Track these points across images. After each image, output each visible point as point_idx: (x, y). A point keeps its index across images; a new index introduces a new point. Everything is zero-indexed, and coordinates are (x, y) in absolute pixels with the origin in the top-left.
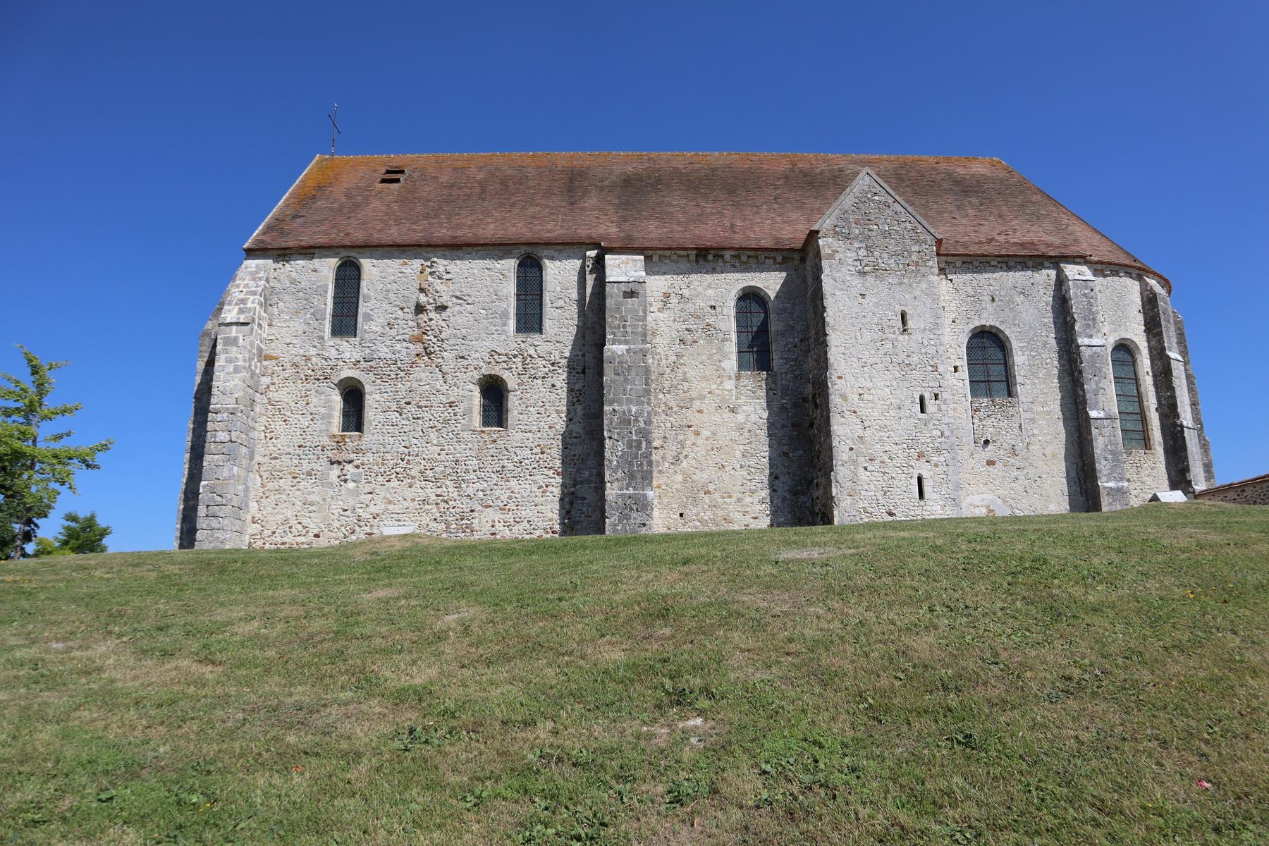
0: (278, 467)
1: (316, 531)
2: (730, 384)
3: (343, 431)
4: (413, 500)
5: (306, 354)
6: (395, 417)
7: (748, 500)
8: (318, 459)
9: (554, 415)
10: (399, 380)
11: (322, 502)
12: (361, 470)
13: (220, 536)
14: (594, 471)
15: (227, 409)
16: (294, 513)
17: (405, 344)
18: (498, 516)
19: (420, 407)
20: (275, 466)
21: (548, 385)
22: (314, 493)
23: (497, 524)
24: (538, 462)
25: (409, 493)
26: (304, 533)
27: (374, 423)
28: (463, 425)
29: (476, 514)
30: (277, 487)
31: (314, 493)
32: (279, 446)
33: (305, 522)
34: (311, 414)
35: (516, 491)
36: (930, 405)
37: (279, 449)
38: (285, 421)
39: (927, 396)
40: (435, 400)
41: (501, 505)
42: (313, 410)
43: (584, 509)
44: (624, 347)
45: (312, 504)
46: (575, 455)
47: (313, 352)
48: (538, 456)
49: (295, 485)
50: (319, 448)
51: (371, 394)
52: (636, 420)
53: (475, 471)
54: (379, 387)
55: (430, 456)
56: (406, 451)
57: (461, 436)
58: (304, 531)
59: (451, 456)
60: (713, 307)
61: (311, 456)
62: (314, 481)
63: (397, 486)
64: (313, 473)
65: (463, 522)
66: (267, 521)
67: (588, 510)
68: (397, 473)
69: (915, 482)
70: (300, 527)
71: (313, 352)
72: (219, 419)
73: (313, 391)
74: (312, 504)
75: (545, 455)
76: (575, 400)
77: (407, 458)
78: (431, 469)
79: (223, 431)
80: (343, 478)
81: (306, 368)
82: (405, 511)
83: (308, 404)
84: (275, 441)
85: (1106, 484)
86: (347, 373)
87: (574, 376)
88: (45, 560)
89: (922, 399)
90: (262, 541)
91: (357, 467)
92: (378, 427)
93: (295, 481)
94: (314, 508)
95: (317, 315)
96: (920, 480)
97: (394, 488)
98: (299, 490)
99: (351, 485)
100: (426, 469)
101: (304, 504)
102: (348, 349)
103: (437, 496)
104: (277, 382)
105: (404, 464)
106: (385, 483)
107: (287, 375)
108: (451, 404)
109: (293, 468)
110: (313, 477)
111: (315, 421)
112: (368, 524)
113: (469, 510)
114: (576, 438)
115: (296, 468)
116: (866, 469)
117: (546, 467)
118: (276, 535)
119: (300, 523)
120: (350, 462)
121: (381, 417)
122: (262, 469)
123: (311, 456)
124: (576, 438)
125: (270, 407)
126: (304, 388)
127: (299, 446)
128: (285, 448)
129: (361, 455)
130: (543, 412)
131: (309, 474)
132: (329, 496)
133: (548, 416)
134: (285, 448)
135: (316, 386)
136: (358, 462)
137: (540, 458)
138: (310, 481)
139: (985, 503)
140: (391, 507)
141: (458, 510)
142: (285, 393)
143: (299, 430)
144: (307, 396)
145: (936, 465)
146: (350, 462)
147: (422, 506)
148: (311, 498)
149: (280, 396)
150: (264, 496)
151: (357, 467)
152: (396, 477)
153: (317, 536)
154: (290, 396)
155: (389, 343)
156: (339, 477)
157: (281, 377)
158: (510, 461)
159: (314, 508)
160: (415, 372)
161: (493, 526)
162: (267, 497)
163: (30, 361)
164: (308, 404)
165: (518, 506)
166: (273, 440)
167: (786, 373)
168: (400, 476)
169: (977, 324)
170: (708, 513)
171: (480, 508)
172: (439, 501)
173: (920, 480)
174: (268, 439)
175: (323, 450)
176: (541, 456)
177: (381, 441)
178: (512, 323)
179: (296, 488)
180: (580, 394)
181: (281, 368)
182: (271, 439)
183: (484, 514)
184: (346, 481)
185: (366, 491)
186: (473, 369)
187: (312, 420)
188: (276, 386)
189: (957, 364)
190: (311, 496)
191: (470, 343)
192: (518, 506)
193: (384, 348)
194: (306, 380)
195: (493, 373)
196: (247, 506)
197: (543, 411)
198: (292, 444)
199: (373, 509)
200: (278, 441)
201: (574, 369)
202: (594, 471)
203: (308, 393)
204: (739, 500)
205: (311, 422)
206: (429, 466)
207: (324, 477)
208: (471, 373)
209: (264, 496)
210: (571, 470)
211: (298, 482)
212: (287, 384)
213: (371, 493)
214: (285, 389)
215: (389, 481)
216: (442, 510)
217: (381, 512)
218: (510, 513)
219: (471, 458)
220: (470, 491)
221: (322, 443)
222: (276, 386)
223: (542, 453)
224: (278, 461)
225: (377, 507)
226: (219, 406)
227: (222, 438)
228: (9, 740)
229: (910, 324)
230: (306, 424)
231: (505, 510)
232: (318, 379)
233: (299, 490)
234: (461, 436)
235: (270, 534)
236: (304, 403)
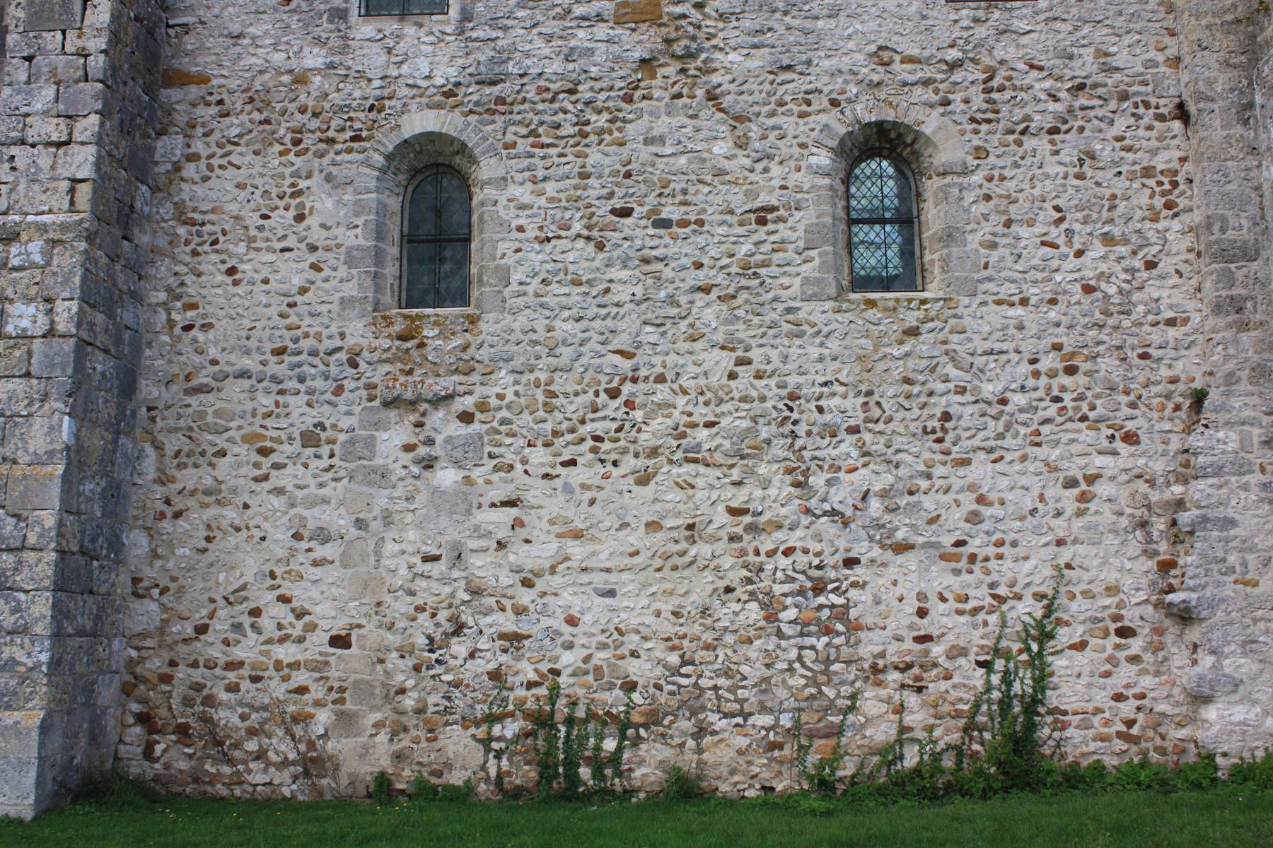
0: (210, 419)
1: (339, 627)
4: (653, 526)
5: (293, 64)
6: (578, 255)
8: (339, 390)
9: (1098, 250)
10: (593, 138)
11: (354, 532)
12: (476, 427)
13: (21, 656)
14: (1256, 431)
15: (43, 228)
16: (267, 568)
17: (602, 31)
18: (941, 578)
19: (664, 224)
20: (202, 415)
21: (1069, 153)
22: (325, 501)
23: (936, 608)
24: (1057, 399)
25: (640, 504)
26: (297, 632)
27: (516, 276)
28: (806, 281)
29: (859, 573)
30: (208, 482)
31: (325, 501)
32: (213, 352)
33: (299, 592)
34: (313, 249)
35: (993, 496)
37: (214, 362)
38: (232, 271)
40: (709, 200)
41: (947, 540)
42: (317, 236)
43: (1233, 559)
45: (323, 536)
46: (1174, 380)
47: (314, 58)
48: (1055, 383)
49: (266, 478)
50: (342, 356)
53: (854, 430)
54: (526, 162)
55: (702, 381)
56: (625, 365)
57: (802, 315)
58: (300, 624)
59: (772, 382)
61: (319, 384)
62: (325, 462)
63: (597, 481)
64: (323, 436)
65: (821, 600)
66: (181, 590)
67: (1245, 564)
68: (597, 439)
70: (281, 611)
71: (314, 58)
72: (15, 262)
73: (317, 179)
74: (323, 536)
75: (1081, 379)
76: (1159, 202)
77: (627, 389)
78: (710, 425)
79: (29, 300)
80: (423, 451)
81: (292, 107)
82: (628, 561)
83: (300, 218)
84: (201, 337)
86: (420, 122)
87: (1150, 128)
90: (166, 655)
91: (466, 418)
92: (530, 289)
93: (266, 462)
97: (584, 487)
98: (279, 491)
99: (447, 476)
100: (693, 426)
101: (297, 537)
103: (733, 512)
104: (204, 153)
105: (613, 408)
106: (560, 470)
107: (234, 132)
108: (762, 216)
109: (258, 420)
110: (325, 450)
111: (327, 272)
112: (507, 603)
113: (839, 557)
114: (1171, 322)
115: (269, 422)
117: (1084, 418)
118: (209, 637)
119: (284, 599)
120: (440, 401)
121: (536, 257)
122: (160, 424)
123: (319, 384)
124: (1171, 322)
125: (182, 231)
126: (288, 171)
127: (280, 352)
128: (232, 358)
129: (475, 377)
130: (1061, 241)
131: (310, 439)
132: (376, 512)
133: (1079, 254)
134: (232, 358)
135: (326, 160)
136: (468, 403)
137: (1063, 389)
138: (315, 464)
140: (576, 550)
141: (801, 559)
142: (229, 186)
143: (275, 300)
144: (300, 193)
146: (440, 401)
147: (683, 545)
148: (315, 517)
149: (213, 195)
150: (169, 511)
151: (466, 418)
152: (594, 450)
153: (340, 641)
154: (243, 195)
155: (551, 27)
156: (408, 448)
157: (217, 135)
158: (969, 397)
160: (640, 114)
161: (922, 613)
162: (178, 515)
164: (300, 218)
165: (1000, 543)
166: (194, 332)
168: (606, 446)
171: (876, 552)
172: (739, 530)
174: (178, 330)
175: (354, 365)
176: (1066, 380)
177: (541, 335)
179: (266, 485)
180: (1175, 185)
181: (214, 110)
182: (188, 328)
183: (892, 572)
184: (429, 464)
185: (498, 495)
186: (826, 103)
187: (316, 267)
188: (203, 164)
190: (316, 511)
191: (808, 24)
192: (1000, 543)
193: (539, 42)
194: (297, 142)
195: (890, 115)
196: (116, 545)
197: (1055, 234)
198: (253, 343)
199: (520, 555)
200: (211, 335)
201: (1147, 105)
202: (1256, 431)
203: (303, 184)
205: (313, 275)
206: (702, 413)
207: (361, 448)
208: (823, 118)
209: (169, 511)
210: (1167, 426)
211: (277, 466)
212: (235, 159)
213: (511, 503)
214: (231, 172)
215: (573, 463)
216: (751, 558)
217: (547, 564)
218: (977, 568)
219: (837, 388)
220: (841, 497)
221: (350, 341)
222: (203, 164)
223: (1071, 371)
224: (210, 398)
225: (533, 549)
226: (17, 218)
227: (25, 323)
228: (154, 210)
230: (297, 281)
231: (957, 558)
232: (332, 141)
233: (279, 491)
234: (802, 315)
235: (190, 631)
236: (292, 213)
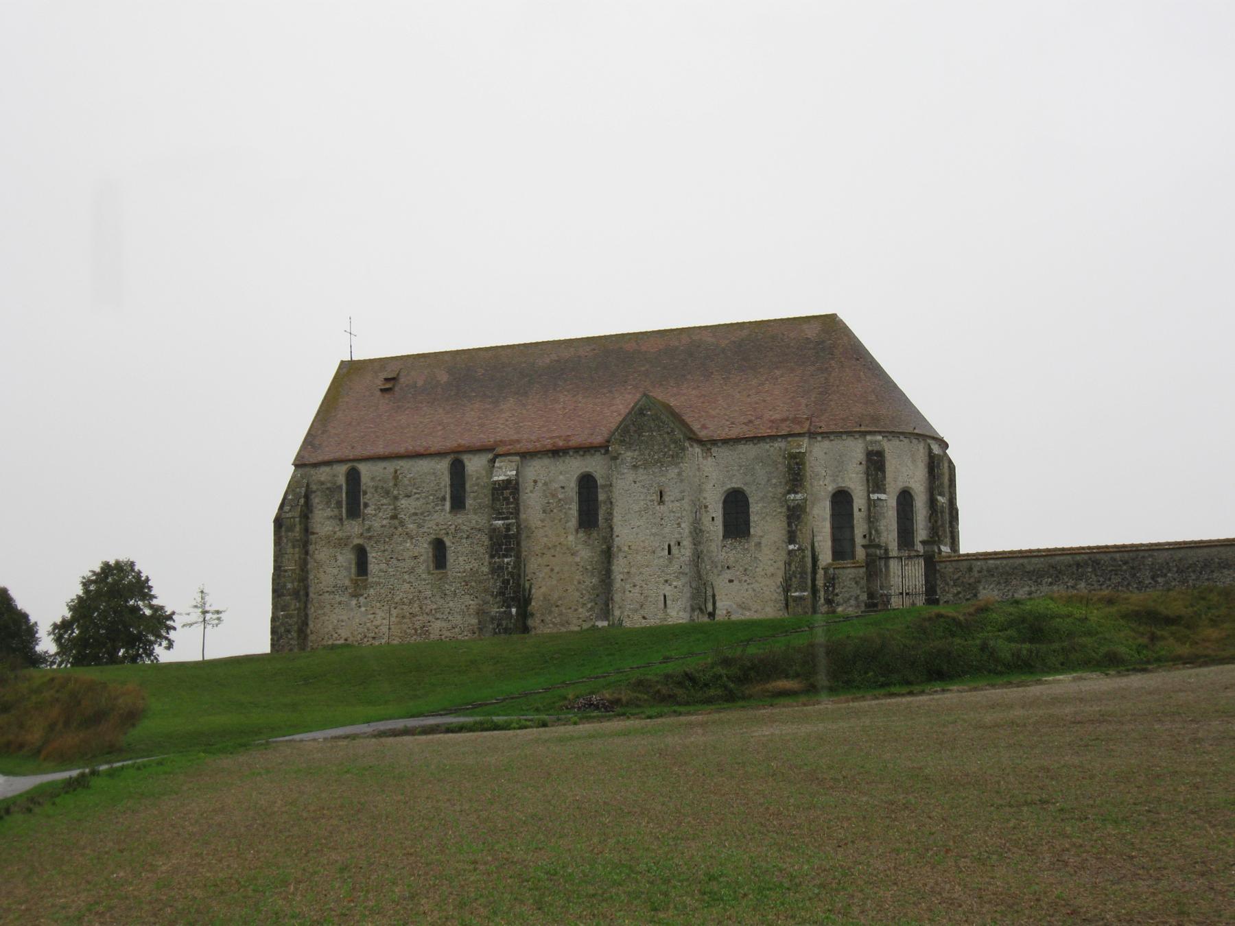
2: (571, 538)
3: (359, 575)
7: (580, 610)
36: (675, 550)
39: (672, 544)
44: (500, 522)
45: (342, 621)
51: (371, 553)
52: (507, 568)
60: (563, 488)
69: (662, 598)
85: (793, 594)
86: (357, 541)
88: (1057, 690)
89: (669, 546)
94: (343, 624)
95: (339, 504)
96: (665, 596)
102: (354, 528)
108: (415, 557)
116: (630, 591)
131: (340, 603)
139: (725, 607)
145: (676, 587)
148: (341, 618)
159: (343, 624)
161: (440, 631)
163: (224, 611)
167: (605, 528)
169: (729, 487)
170: (558, 619)
171: (433, 620)
173: (665, 596)
178: (448, 505)
189: (714, 516)
204: (576, 610)
206: (405, 596)
229: (666, 498)
